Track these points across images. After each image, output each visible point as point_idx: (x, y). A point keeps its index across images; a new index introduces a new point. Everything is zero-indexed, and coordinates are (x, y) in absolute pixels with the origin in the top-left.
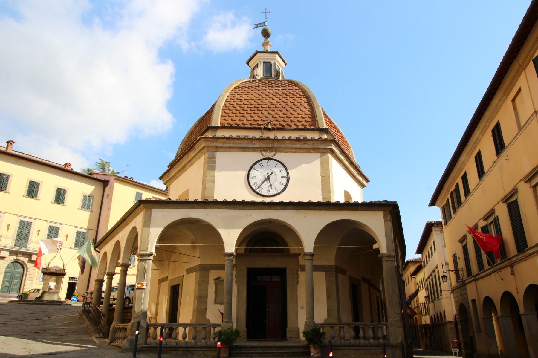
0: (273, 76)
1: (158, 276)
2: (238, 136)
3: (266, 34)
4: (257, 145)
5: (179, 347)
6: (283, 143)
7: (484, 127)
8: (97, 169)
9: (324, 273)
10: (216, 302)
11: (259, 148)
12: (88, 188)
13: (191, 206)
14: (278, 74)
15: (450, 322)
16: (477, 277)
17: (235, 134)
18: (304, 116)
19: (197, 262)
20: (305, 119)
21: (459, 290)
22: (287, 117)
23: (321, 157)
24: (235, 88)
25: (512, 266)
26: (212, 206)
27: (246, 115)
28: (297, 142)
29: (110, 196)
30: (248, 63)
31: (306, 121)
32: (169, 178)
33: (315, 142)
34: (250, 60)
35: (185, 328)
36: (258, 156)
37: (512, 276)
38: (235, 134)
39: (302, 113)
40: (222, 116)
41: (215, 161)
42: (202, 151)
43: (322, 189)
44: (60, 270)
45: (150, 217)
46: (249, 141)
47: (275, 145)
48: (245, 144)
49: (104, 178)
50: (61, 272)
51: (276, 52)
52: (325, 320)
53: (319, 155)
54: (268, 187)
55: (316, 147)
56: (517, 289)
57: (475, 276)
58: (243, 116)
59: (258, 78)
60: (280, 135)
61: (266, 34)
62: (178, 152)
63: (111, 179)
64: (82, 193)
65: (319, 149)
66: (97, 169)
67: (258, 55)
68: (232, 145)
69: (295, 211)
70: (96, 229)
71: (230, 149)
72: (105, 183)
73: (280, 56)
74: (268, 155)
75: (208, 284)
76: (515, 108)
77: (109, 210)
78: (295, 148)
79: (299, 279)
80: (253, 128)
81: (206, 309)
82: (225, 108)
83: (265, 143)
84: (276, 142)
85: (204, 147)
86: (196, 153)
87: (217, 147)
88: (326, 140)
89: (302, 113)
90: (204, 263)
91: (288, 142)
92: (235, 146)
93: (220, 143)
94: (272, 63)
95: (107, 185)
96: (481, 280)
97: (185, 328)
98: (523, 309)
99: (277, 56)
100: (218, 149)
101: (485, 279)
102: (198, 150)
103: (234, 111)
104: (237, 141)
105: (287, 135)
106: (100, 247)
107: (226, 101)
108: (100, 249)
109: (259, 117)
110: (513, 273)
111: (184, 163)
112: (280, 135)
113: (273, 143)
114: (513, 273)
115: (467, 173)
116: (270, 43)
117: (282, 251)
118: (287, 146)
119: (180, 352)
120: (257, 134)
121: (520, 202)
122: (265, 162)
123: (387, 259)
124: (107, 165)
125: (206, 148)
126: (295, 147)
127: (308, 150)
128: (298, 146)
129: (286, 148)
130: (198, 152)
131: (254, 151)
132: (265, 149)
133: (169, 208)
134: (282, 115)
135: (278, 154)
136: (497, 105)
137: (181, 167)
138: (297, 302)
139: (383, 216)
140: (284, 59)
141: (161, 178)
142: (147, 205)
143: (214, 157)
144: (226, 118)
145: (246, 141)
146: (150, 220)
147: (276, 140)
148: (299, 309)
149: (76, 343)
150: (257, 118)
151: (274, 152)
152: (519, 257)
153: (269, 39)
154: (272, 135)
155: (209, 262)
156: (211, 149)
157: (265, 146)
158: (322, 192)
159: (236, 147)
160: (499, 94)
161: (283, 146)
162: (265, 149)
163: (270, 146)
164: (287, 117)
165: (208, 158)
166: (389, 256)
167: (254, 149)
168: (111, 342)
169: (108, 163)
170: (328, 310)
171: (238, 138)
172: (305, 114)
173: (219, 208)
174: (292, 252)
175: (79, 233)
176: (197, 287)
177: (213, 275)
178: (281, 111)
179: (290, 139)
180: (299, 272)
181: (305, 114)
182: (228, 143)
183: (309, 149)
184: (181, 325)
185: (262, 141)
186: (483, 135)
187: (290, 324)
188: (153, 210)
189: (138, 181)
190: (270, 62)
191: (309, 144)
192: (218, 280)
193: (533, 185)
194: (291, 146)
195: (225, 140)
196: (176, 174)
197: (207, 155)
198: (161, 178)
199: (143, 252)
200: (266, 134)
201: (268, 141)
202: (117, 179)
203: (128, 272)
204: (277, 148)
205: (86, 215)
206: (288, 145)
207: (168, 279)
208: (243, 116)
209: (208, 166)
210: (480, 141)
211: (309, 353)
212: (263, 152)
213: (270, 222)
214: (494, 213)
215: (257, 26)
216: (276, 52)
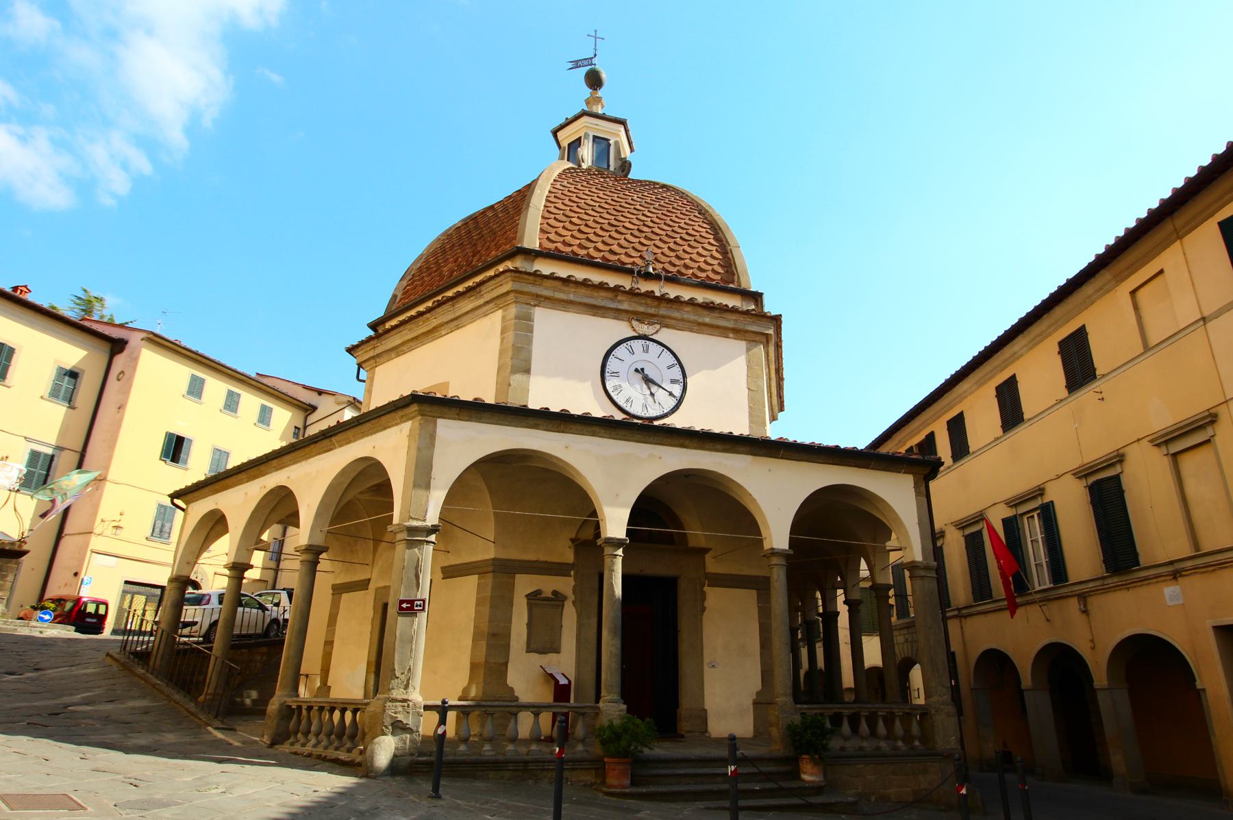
0: (612, 169)
1: (330, 576)
2: (585, 280)
3: (594, 80)
4: (625, 306)
5: (507, 762)
6: (678, 310)
7: (1040, 335)
8: (72, 309)
9: (754, 592)
10: (529, 650)
11: (626, 311)
12: (72, 353)
13: (531, 421)
14: (625, 166)
15: (849, 689)
16: (964, 612)
17: (563, 271)
18: (710, 260)
19: (486, 552)
20: (712, 268)
21: (905, 631)
22: (678, 257)
23: (748, 350)
24: (560, 175)
25: (1083, 597)
26: (579, 427)
27: (592, 237)
28: (705, 312)
29: (126, 377)
30: (555, 133)
31: (713, 271)
32: (377, 351)
33: (741, 318)
34: (562, 127)
35: (537, 715)
36: (621, 329)
37: (1083, 616)
38: (563, 271)
39: (705, 253)
40: (542, 231)
41: (532, 326)
42: (498, 302)
43: (750, 415)
44: (13, 543)
45: (433, 437)
46: (610, 295)
47: (663, 311)
48: (600, 299)
49: (115, 333)
50: (16, 548)
51: (622, 122)
52: (758, 693)
53: (742, 345)
54: (646, 399)
55: (740, 326)
56: (1092, 641)
57: (959, 610)
58: (588, 239)
59: (584, 166)
60: (673, 291)
61: (594, 80)
62: (394, 297)
63: (135, 340)
64: (56, 361)
65: (747, 331)
66: (72, 309)
67: (585, 119)
68: (572, 297)
69: (750, 458)
70: (80, 449)
71: (566, 305)
72: (117, 346)
73: (627, 131)
74: (644, 329)
75: (511, 604)
76: (1136, 307)
77: (121, 407)
78: (700, 324)
79: (706, 604)
80: (605, 266)
81: (506, 664)
82: (547, 215)
83: (641, 304)
84: (664, 304)
85: (508, 293)
86: (482, 301)
87: (538, 296)
88: (747, 313)
89: (705, 253)
90: (503, 555)
91: (688, 309)
92: (579, 300)
93: (547, 288)
94: (611, 142)
95: (121, 350)
96: (969, 620)
97: (537, 715)
98: (1029, 677)
99: (622, 129)
100: (541, 300)
101: (991, 617)
102: (488, 297)
103: (568, 225)
104: (583, 291)
105: (686, 294)
106: (190, 496)
107: (547, 201)
108: (187, 503)
109: (621, 246)
110: (1085, 612)
111: (434, 323)
112: (673, 291)
113: (658, 306)
114: (1085, 612)
115: (965, 415)
116: (604, 101)
117: (669, 539)
118: (686, 316)
119: (508, 774)
120: (626, 282)
121: (1125, 481)
122: (637, 345)
123: (922, 573)
124: (97, 305)
125: (512, 296)
126: (700, 320)
127: (723, 332)
128: (707, 320)
129: (683, 320)
130: (487, 303)
131: (615, 318)
132: (639, 317)
133: (479, 420)
134: (666, 251)
135: (664, 330)
136: (1089, 297)
137: (425, 329)
138: (702, 654)
139: (912, 484)
140: (633, 139)
141: (351, 350)
142: (427, 408)
143: (529, 318)
144: (553, 236)
145: (603, 294)
146: (432, 445)
147: (663, 299)
148: (706, 668)
149: (259, 757)
150: (615, 248)
151: (658, 326)
152: (1109, 581)
153: (600, 93)
154: (657, 288)
155: (514, 554)
156: (523, 298)
157: (641, 309)
158: (751, 422)
159: (580, 304)
160: (1104, 276)
161: (677, 315)
162: (642, 317)
163: (652, 311)
164: (678, 257)
165: (517, 317)
166: (927, 568)
167: (617, 314)
168: (272, 745)
169: (100, 300)
170: (763, 672)
171: (585, 284)
172: (712, 256)
173: (593, 435)
174: (692, 543)
175: (35, 456)
176: (486, 609)
177: (524, 585)
178: (665, 242)
179: (691, 302)
180: (706, 589)
181: (712, 256)
182: (563, 292)
183: (726, 329)
184: (527, 707)
185: (636, 299)
186: (1031, 348)
187: (686, 702)
188: (440, 422)
189: (200, 352)
190: (608, 140)
191: (728, 320)
192: (534, 598)
193: (1173, 451)
194: (692, 317)
195: (558, 284)
196: (403, 344)
197: (513, 310)
198: (351, 350)
199: (415, 523)
200: (645, 286)
201: (649, 301)
202: (149, 340)
203: (319, 567)
204: (663, 317)
205: (59, 411)
206: (688, 314)
207: (372, 586)
208: (588, 239)
209: (516, 336)
210: (1018, 359)
211: (795, 774)
212: (635, 323)
213: (687, 476)
214: (1042, 495)
215: (577, 64)
216: (622, 122)
